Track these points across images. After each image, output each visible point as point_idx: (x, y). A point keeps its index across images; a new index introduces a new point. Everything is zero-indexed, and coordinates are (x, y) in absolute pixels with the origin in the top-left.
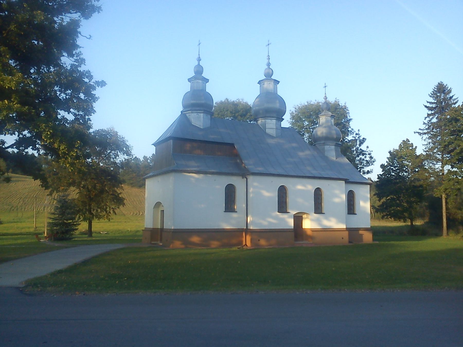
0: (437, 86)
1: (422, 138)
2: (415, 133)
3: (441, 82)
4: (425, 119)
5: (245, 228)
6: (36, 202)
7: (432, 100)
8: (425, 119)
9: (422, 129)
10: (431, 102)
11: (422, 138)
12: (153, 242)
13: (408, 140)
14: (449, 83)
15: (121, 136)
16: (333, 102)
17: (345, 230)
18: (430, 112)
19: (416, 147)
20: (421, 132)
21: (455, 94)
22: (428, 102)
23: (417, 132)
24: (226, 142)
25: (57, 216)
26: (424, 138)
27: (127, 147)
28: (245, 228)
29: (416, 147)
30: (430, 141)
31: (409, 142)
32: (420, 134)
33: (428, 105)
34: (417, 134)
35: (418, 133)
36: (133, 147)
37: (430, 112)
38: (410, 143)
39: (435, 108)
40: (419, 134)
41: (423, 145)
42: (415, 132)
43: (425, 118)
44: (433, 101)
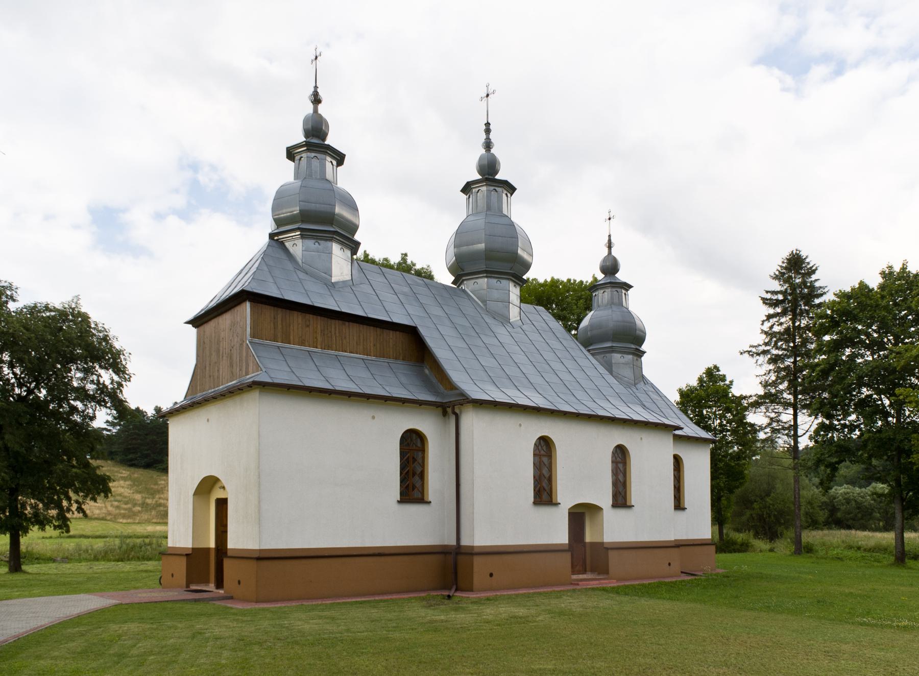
0: (787, 259)
1: (756, 362)
2: (741, 353)
3: (797, 250)
4: (762, 324)
5: (453, 542)
6: (281, 348)
7: (776, 286)
8: (762, 324)
9: (756, 344)
10: (774, 291)
11: (756, 362)
12: (193, 587)
13: (716, 368)
14: (812, 258)
15: (100, 325)
16: (590, 281)
17: (567, 548)
18: (771, 311)
19: (731, 382)
20: (754, 350)
21: (819, 279)
22: (767, 292)
23: (745, 352)
24: (276, 381)
25: (721, 412)
26: (759, 363)
27: (117, 354)
28: (454, 543)
29: (731, 382)
30: (771, 367)
31: (718, 370)
32: (752, 355)
33: (769, 296)
34: (746, 355)
35: (749, 352)
36: (130, 354)
37: (771, 311)
38: (721, 373)
39: (782, 302)
40: (750, 355)
41: (757, 376)
42: (742, 351)
43: (761, 323)
44: (778, 288)
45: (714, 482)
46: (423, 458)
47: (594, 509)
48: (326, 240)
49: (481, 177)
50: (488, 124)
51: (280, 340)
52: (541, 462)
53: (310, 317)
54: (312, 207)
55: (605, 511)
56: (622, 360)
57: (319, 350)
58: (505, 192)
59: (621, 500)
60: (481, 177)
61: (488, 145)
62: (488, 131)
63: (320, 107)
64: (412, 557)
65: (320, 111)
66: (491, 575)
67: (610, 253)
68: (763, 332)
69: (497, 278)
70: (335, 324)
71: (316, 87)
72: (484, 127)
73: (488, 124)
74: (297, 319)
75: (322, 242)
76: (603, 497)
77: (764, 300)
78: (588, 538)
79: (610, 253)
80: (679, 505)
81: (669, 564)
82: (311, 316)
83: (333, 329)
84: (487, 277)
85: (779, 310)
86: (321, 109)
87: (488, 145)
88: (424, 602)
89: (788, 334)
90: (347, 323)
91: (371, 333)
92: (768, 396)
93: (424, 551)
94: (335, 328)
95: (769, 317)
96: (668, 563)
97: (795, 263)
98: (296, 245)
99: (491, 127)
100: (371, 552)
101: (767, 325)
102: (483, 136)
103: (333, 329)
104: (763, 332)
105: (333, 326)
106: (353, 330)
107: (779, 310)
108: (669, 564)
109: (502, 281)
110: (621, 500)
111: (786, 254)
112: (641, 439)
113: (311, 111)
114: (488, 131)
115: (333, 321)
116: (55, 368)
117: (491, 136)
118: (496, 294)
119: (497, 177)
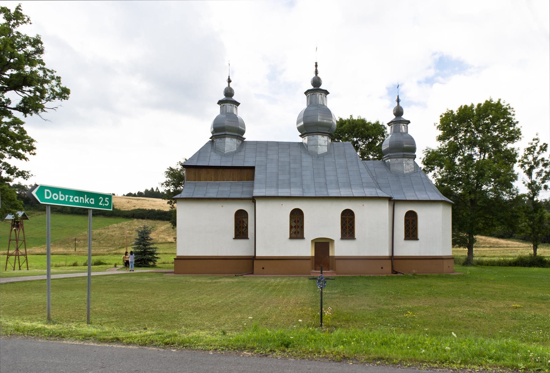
33: (27, 154)
45: (454, 226)
48: (224, 138)
51: (213, 180)
53: (209, 170)
54: (218, 126)
55: (335, 242)
56: (396, 162)
57: (213, 182)
58: (235, 106)
61: (316, 72)
62: (316, 66)
63: (231, 84)
64: (239, 260)
65: (231, 86)
66: (263, 268)
67: (398, 104)
69: (311, 135)
70: (220, 171)
72: (315, 64)
74: (204, 171)
75: (222, 139)
79: (398, 104)
82: (210, 169)
83: (219, 173)
84: (307, 135)
86: (231, 85)
87: (316, 72)
88: (53, 251)
90: (225, 170)
91: (236, 172)
93: (242, 258)
94: (220, 173)
96: (383, 269)
100: (221, 258)
102: (315, 68)
103: (219, 173)
105: (219, 172)
106: (228, 172)
109: (324, 136)
112: (363, 205)
113: (227, 86)
114: (316, 66)
115: (219, 170)
117: (318, 68)
118: (312, 143)
119: (321, 87)
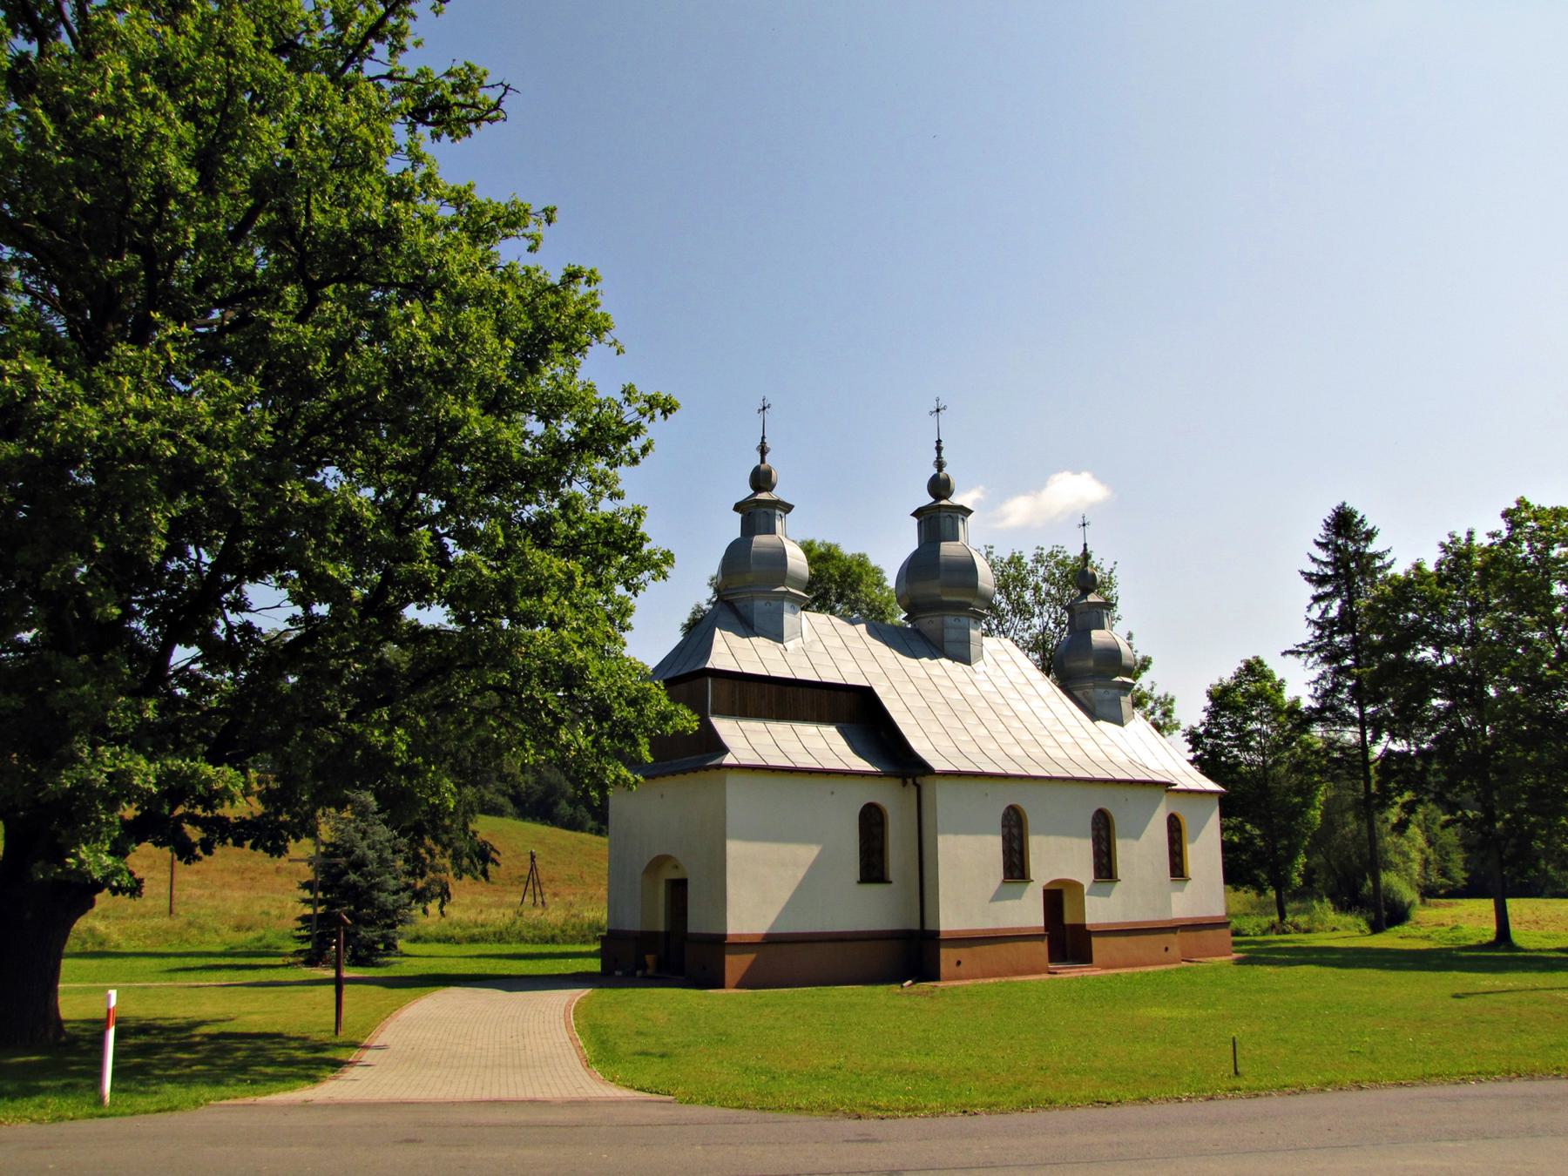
46: (883, 833)
47: (1076, 886)
49: (808, 853)
50: (939, 442)
52: (1010, 832)
59: (1105, 869)
60: (808, 853)
61: (940, 465)
62: (939, 449)
68: (1311, 622)
71: (763, 438)
73: (939, 442)
76: (1082, 871)
77: (1309, 577)
78: (1069, 919)
80: (1178, 869)
81: (1166, 949)
85: (1328, 588)
87: (940, 465)
89: (1346, 621)
92: (1323, 709)
95: (1317, 599)
97: (1343, 523)
98: (530, 249)
99: (943, 445)
101: (1316, 614)
104: (1311, 622)
107: (1328, 588)
108: (1166, 949)
110: (1105, 869)
111: (1327, 513)
114: (939, 449)
116: (313, 797)
117: (943, 454)
